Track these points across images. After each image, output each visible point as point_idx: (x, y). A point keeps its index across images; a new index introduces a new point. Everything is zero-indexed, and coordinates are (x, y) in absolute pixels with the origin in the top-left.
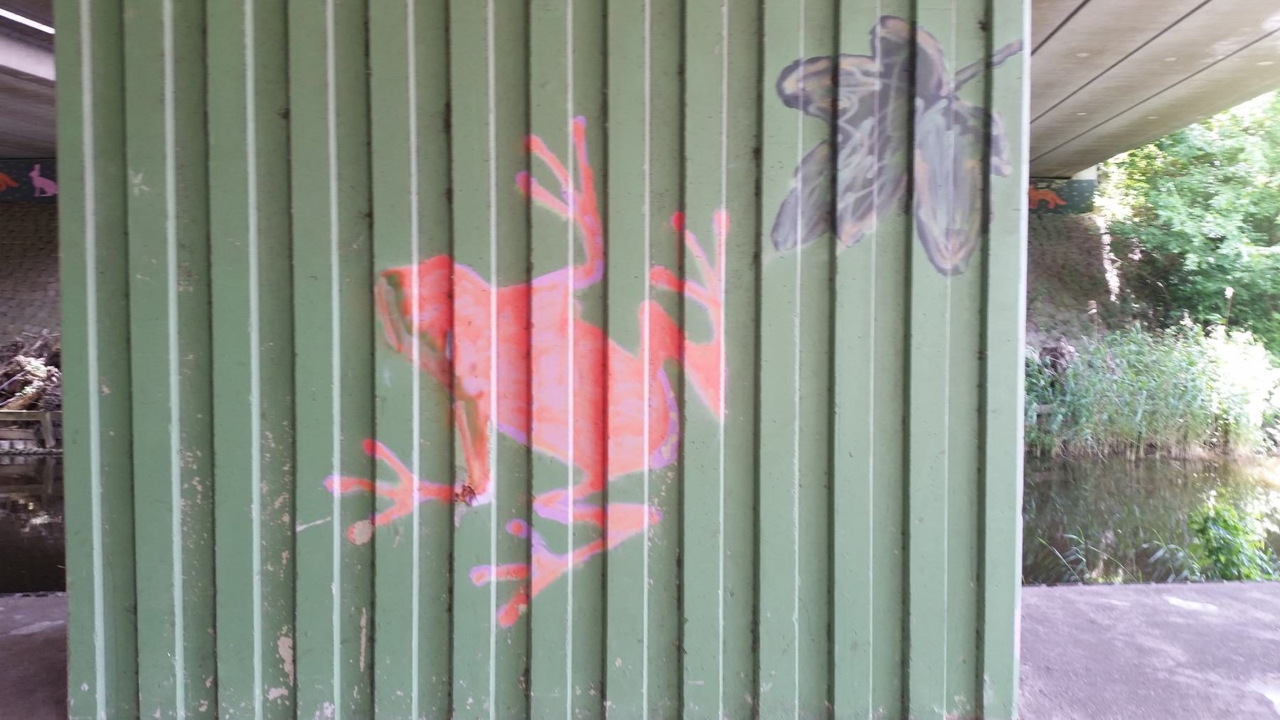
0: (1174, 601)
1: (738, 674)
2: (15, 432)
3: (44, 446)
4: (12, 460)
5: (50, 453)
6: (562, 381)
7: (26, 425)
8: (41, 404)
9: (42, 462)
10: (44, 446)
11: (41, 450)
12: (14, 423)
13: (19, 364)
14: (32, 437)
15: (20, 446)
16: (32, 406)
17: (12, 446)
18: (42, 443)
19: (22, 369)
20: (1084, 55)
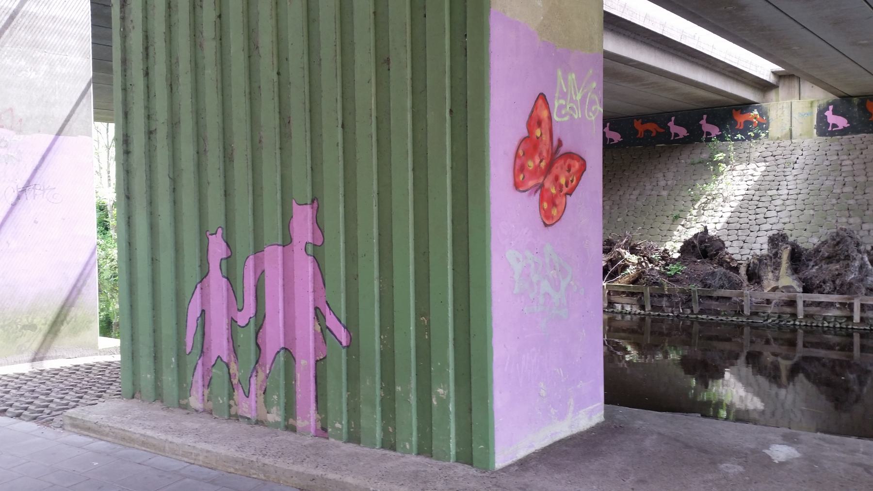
0: (222, 450)
1: (209, 286)
2: (624, 299)
3: (644, 310)
4: (623, 317)
5: (649, 315)
6: (444, 303)
7: (632, 294)
8: (642, 281)
9: (643, 319)
10: (644, 310)
11: (642, 312)
12: (623, 293)
13: (619, 253)
14: (635, 302)
15: (628, 308)
16: (635, 281)
17: (623, 308)
18: (643, 307)
19: (622, 257)
20: (408, 446)
